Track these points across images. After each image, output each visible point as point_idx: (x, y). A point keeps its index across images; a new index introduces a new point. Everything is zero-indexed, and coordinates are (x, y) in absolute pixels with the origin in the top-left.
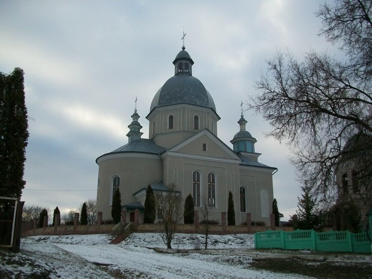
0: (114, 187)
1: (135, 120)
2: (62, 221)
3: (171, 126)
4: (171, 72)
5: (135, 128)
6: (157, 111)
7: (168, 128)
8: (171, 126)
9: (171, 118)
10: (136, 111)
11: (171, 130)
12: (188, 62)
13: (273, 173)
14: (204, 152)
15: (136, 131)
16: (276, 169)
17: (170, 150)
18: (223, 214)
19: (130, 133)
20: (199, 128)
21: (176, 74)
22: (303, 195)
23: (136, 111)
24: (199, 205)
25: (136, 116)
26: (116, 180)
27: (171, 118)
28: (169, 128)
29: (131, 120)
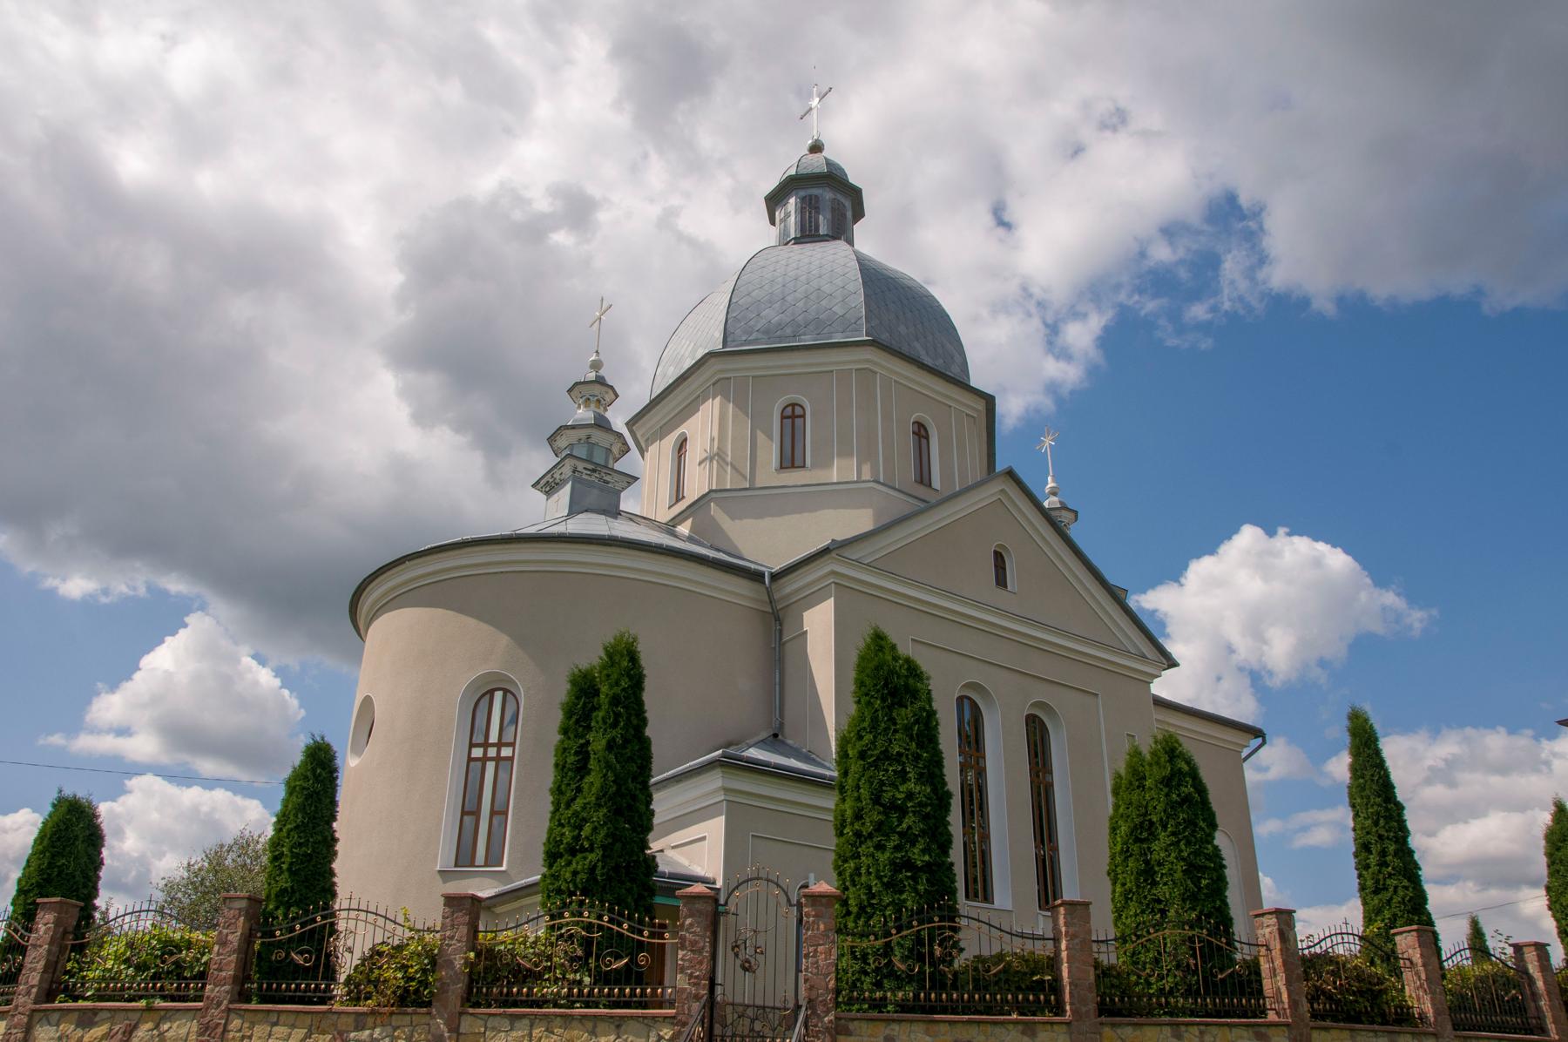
0: (477, 752)
11: (793, 477)
14: (1000, 591)
20: (936, 483)
24: (981, 888)
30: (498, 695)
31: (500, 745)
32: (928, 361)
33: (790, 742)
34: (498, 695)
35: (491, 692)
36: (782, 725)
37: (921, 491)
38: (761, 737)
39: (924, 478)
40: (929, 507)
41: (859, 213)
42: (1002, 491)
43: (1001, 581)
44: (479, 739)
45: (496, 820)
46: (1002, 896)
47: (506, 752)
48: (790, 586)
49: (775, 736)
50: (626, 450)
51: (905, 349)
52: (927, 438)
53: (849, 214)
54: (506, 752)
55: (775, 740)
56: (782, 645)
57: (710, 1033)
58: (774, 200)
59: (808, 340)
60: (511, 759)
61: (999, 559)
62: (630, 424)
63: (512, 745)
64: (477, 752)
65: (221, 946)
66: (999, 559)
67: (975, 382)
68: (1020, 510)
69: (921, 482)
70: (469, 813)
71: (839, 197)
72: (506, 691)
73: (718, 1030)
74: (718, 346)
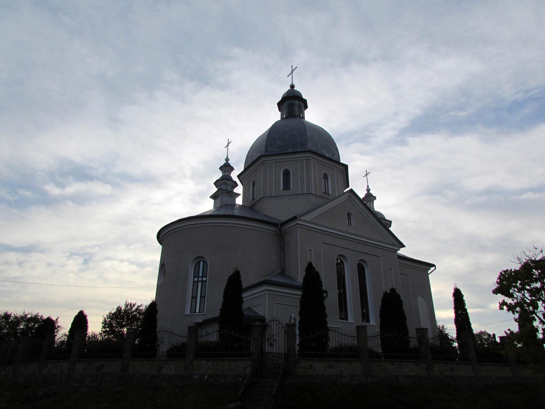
0: (196, 279)
1: (227, 173)
2: (163, 348)
3: (287, 186)
4: (276, 116)
5: (224, 186)
6: (263, 161)
7: (282, 189)
8: (287, 186)
9: (287, 174)
10: (227, 160)
11: (286, 192)
12: (302, 104)
13: (429, 272)
15: (229, 189)
16: (433, 265)
17: (303, 218)
18: (290, 326)
19: (220, 193)
20: (330, 193)
21: (282, 118)
22: (141, 306)
23: (227, 160)
25: (227, 168)
26: (199, 265)
27: (287, 174)
28: (284, 189)
29: (219, 175)
30: (202, 263)
31: (202, 277)
32: (327, 155)
33: (287, 273)
34: (202, 263)
35: (199, 262)
36: (284, 268)
37: (326, 196)
38: (278, 272)
39: (326, 193)
40: (329, 201)
41: (306, 107)
42: (349, 196)
43: (350, 224)
44: (196, 275)
45: (203, 299)
46: (350, 319)
47: (204, 279)
48: (286, 227)
49: (282, 272)
50: (236, 185)
51: (320, 152)
52: (327, 179)
53: (303, 108)
54: (204, 279)
55: (283, 273)
56: (284, 244)
57: (8, 248)
58: (280, 105)
59: (290, 151)
60: (206, 281)
61: (349, 215)
62: (239, 176)
63: (206, 277)
64: (196, 279)
65: (212, 335)
66: (349, 215)
67: (341, 162)
68: (355, 202)
69: (325, 193)
70: (194, 297)
71: (300, 103)
72: (204, 261)
73: (12, 256)
74: (264, 153)
